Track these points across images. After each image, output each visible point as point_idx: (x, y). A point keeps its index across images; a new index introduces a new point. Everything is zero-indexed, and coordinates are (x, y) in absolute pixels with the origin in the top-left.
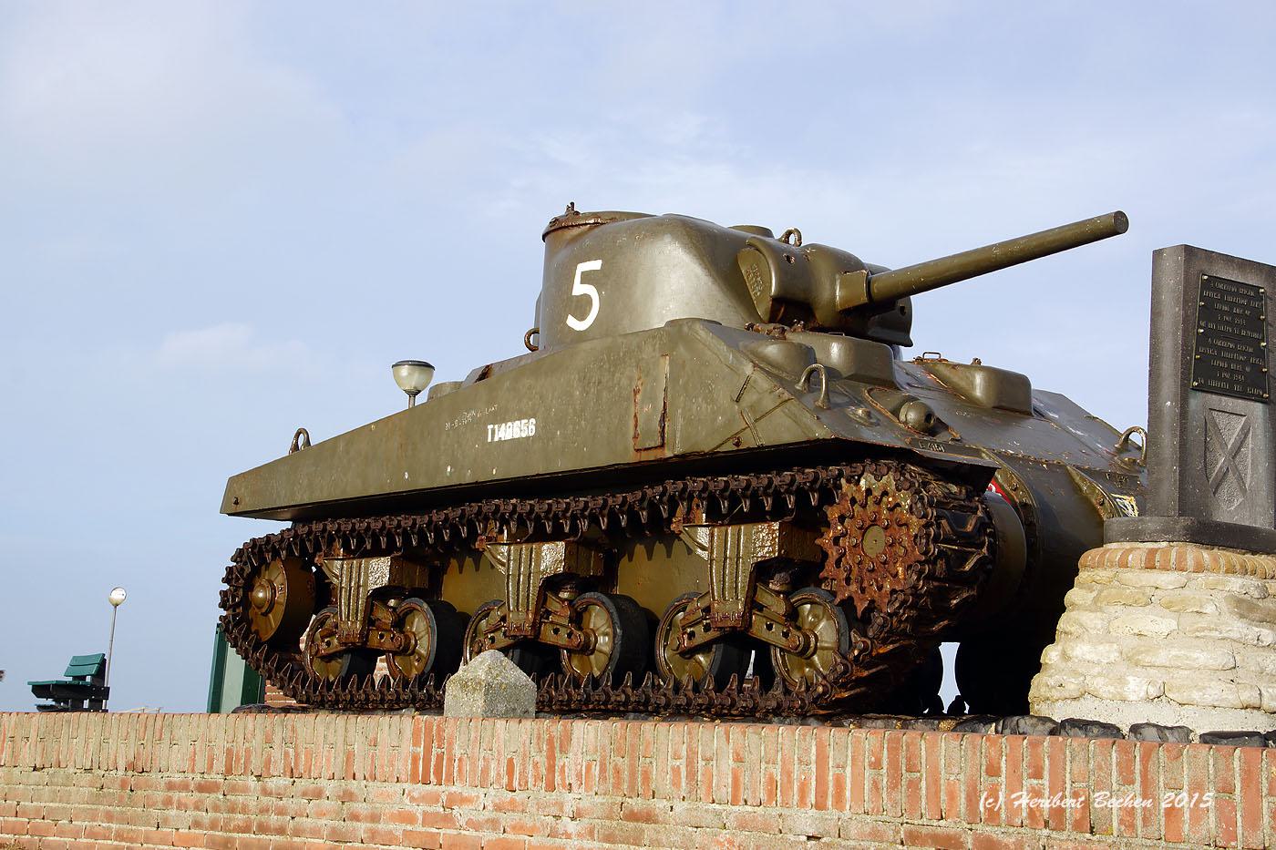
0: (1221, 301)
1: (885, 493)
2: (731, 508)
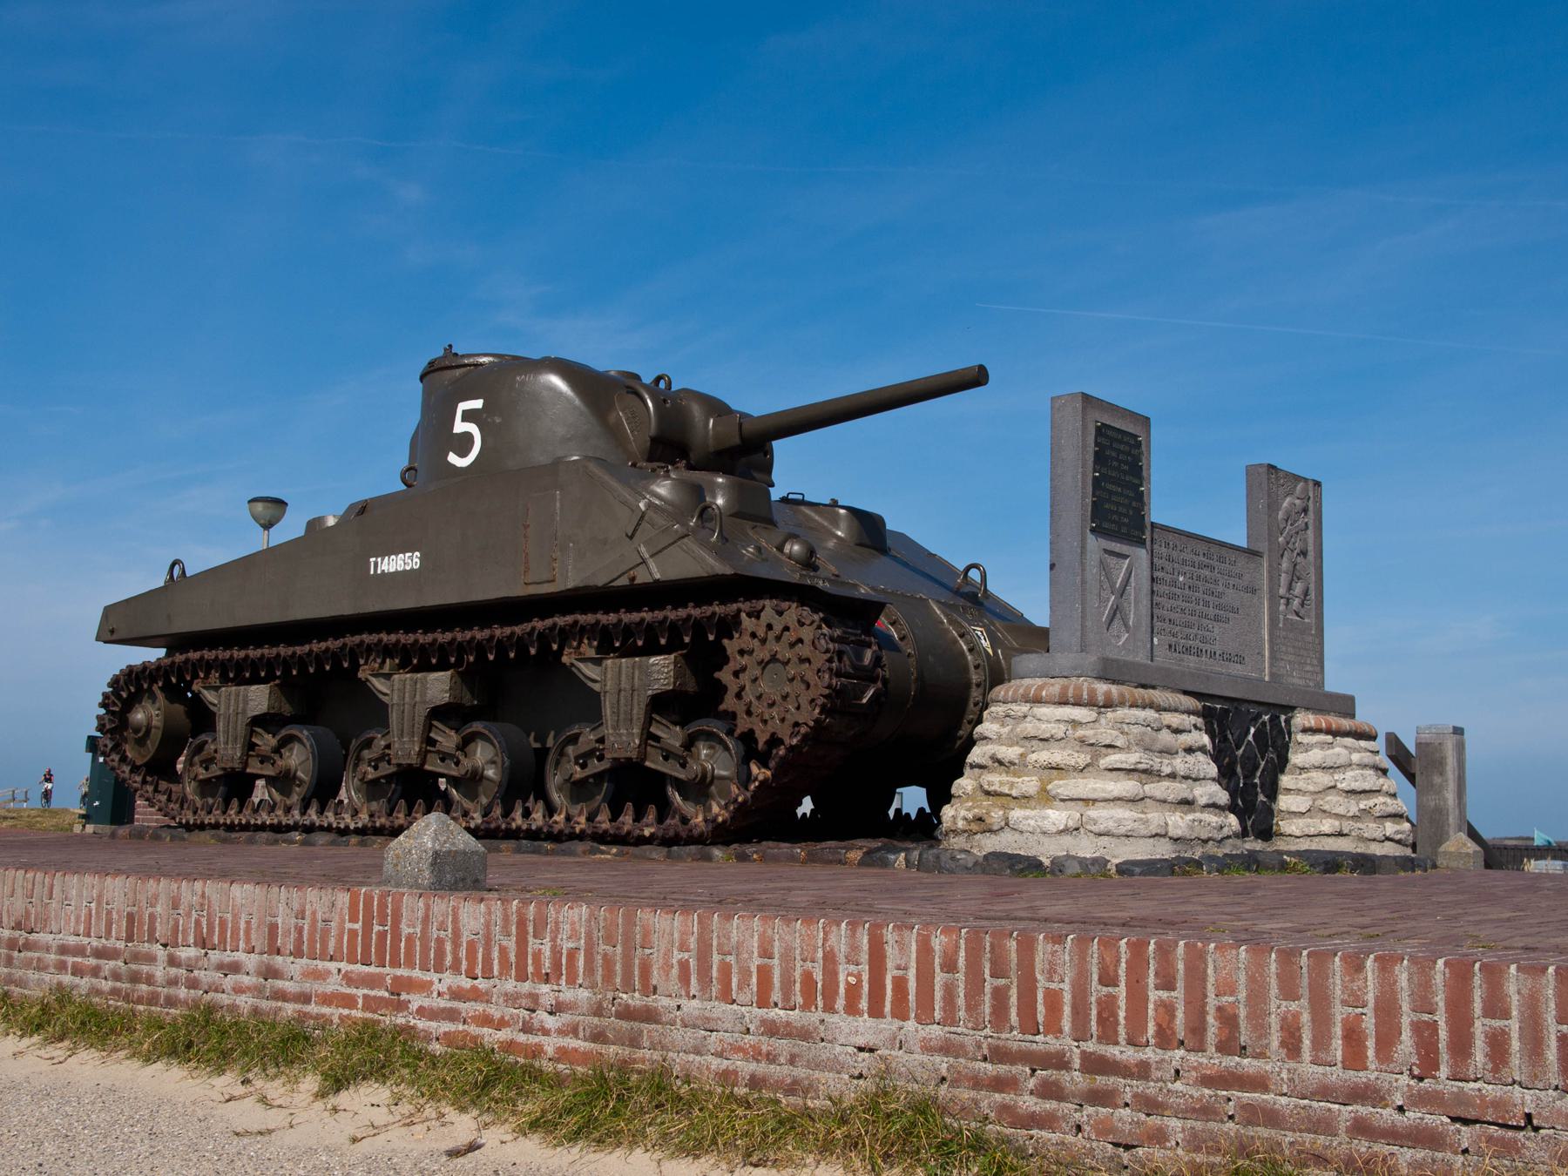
0: (1111, 447)
1: (787, 629)
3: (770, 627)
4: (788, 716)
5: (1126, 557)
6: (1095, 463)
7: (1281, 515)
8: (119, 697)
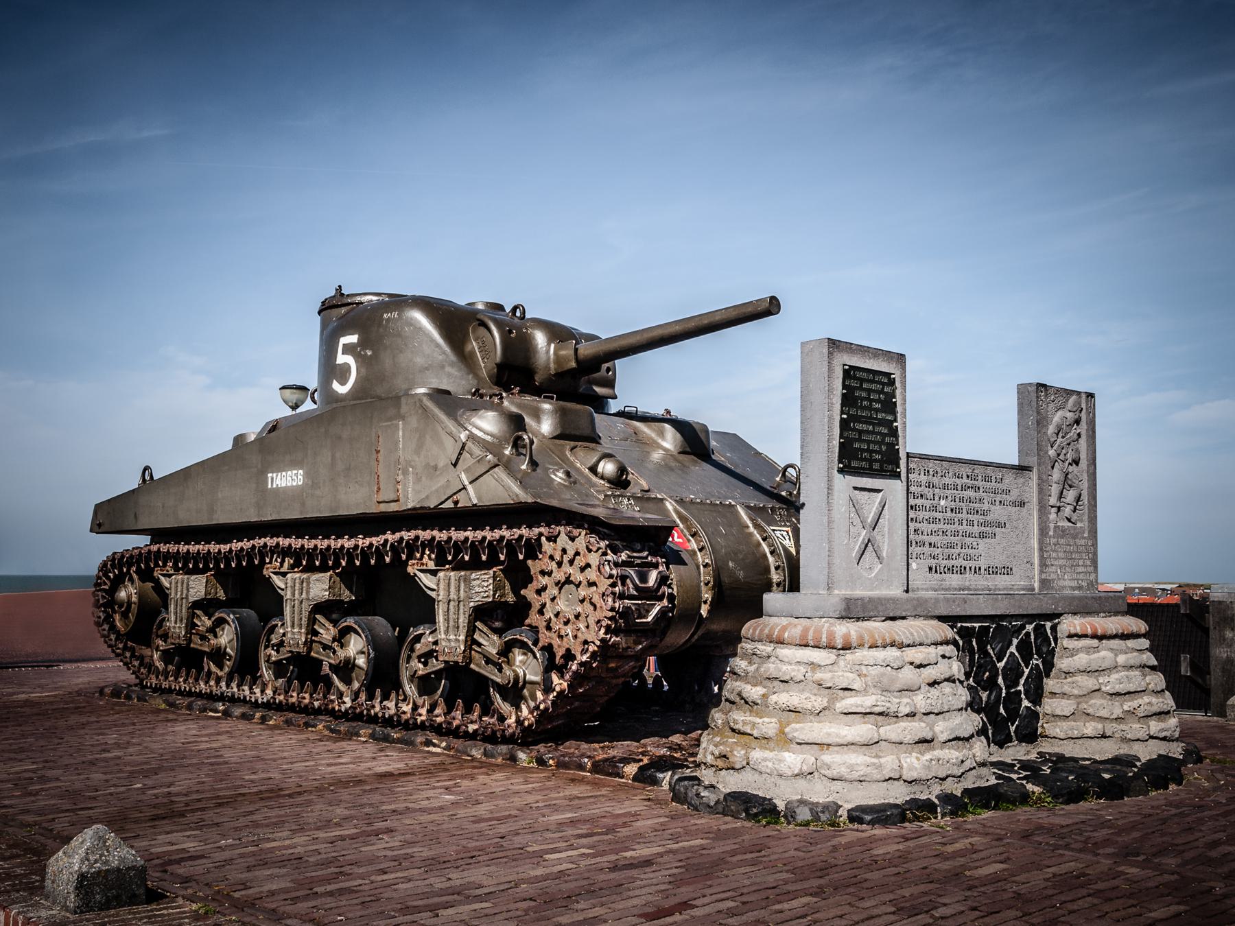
0: (860, 440)
1: (577, 554)
2: (455, 557)
3: (564, 551)
4: (579, 634)
5: (879, 491)
6: (843, 405)
7: (1051, 429)
8: (108, 578)
